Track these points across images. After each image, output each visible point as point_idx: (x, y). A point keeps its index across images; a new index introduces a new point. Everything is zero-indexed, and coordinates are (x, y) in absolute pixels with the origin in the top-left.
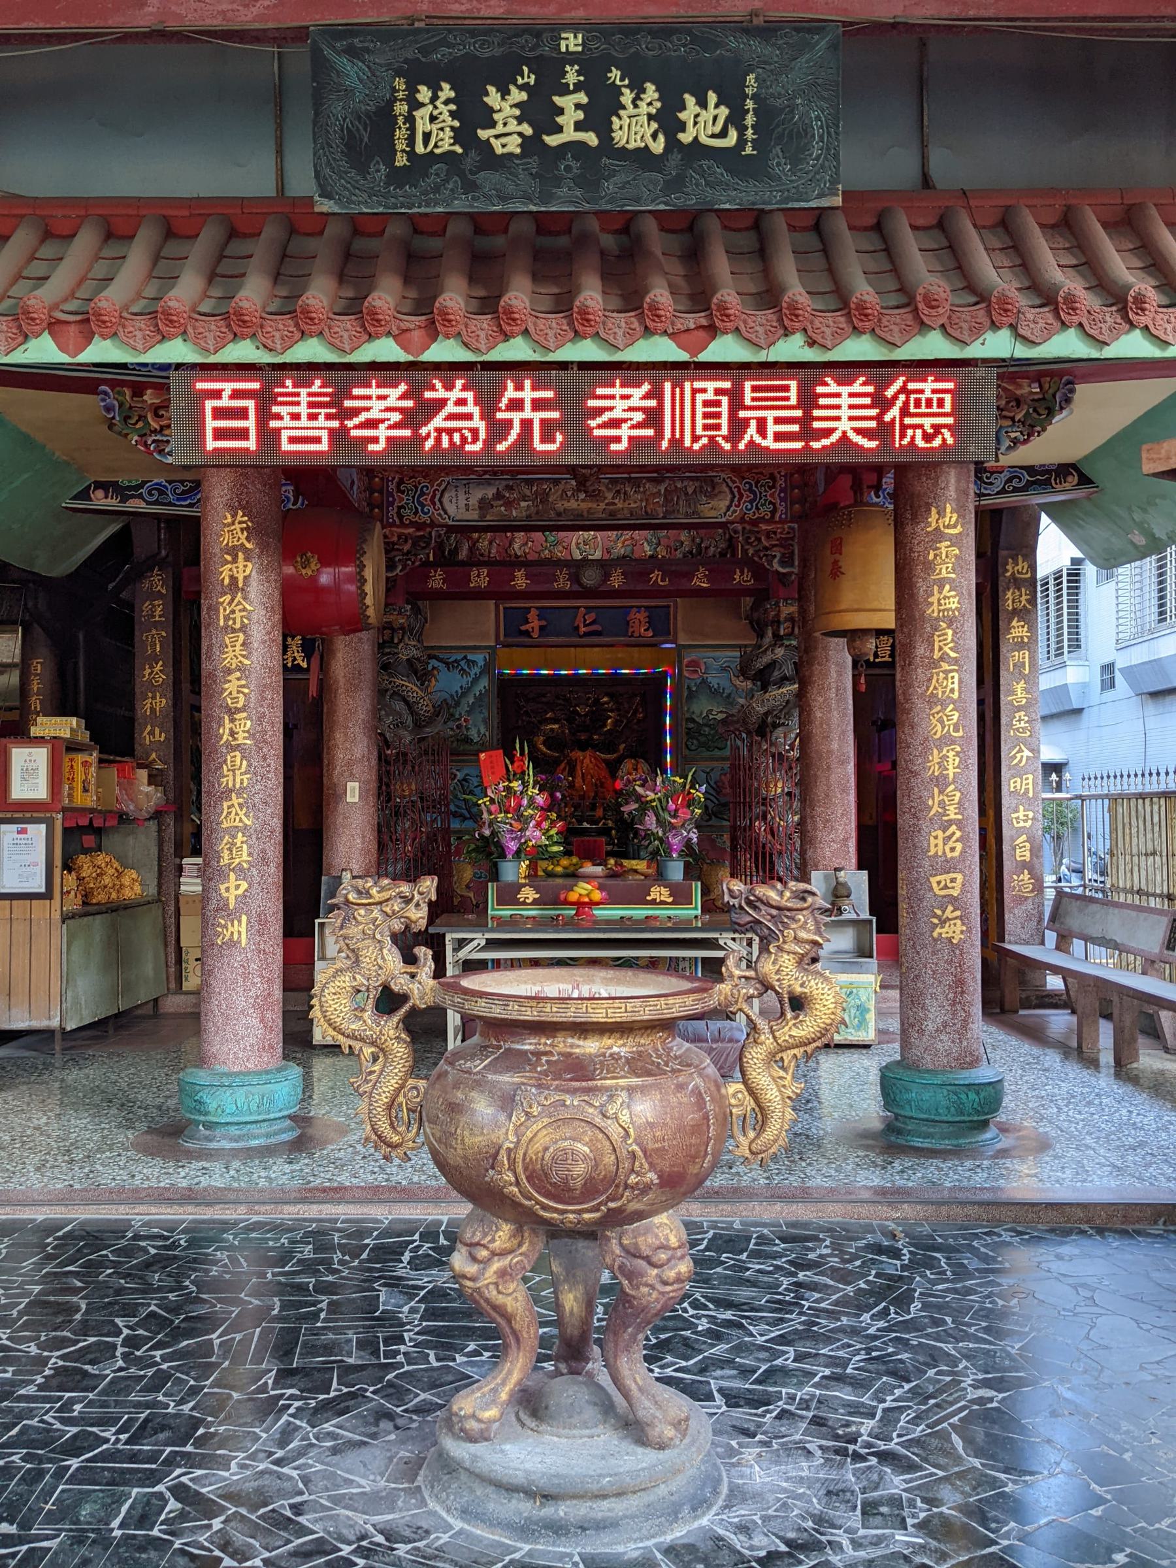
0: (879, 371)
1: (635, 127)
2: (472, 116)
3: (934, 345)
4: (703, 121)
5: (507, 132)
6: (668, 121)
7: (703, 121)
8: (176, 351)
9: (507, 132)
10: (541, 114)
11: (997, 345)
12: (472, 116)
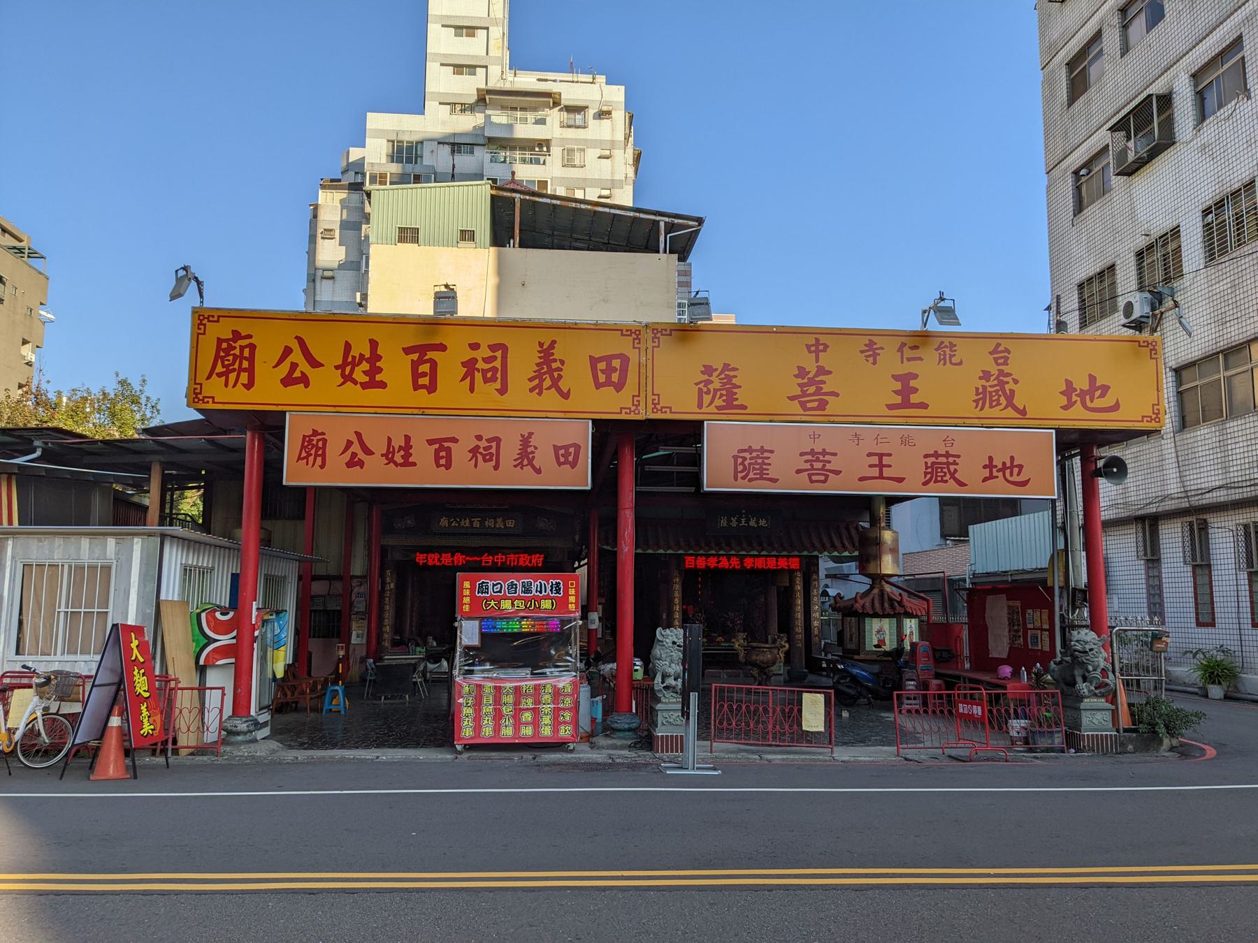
0: (788, 557)
1: (752, 523)
2: (729, 521)
3: (796, 553)
4: (763, 523)
5: (734, 524)
6: (757, 523)
7: (763, 523)
8: (681, 552)
9: (734, 524)
10: (739, 521)
11: (805, 553)
12: (729, 521)
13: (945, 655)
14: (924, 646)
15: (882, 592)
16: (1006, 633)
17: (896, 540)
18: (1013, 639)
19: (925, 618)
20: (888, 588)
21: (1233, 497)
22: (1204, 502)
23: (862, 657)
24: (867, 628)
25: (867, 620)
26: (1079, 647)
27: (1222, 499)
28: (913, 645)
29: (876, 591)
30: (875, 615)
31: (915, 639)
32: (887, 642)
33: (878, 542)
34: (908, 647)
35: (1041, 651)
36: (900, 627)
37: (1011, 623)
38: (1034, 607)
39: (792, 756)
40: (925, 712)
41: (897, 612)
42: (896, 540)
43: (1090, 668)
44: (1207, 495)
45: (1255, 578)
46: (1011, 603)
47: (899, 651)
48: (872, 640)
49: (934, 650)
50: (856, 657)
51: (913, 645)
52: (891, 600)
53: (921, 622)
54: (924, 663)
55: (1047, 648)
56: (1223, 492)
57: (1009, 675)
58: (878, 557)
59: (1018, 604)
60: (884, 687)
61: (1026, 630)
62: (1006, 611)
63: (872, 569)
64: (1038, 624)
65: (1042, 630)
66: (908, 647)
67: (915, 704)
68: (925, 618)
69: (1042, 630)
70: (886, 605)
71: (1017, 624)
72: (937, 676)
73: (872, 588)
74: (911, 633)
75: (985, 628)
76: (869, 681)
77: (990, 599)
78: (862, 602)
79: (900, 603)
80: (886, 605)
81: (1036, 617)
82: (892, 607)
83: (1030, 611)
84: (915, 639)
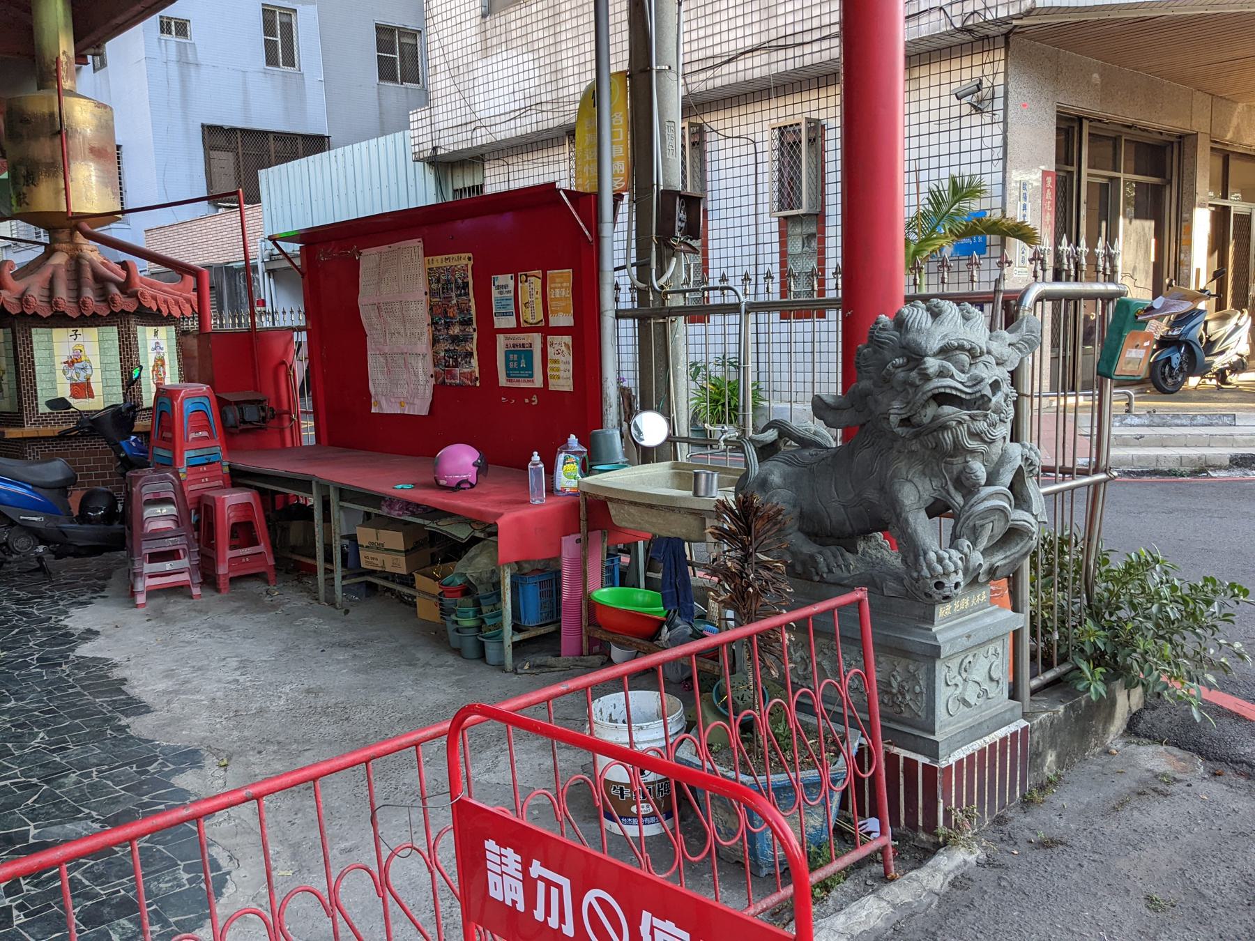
13: (251, 414)
14: (195, 397)
15: (77, 262)
16: (424, 345)
17: (106, 127)
18: (445, 364)
19: (192, 325)
20: (92, 252)
21: (781, 67)
22: (718, 83)
23: (29, 430)
24: (39, 354)
25: (38, 335)
26: (957, 382)
27: (757, 74)
28: (163, 394)
29: (60, 259)
30: (59, 320)
31: (171, 378)
32: (97, 387)
33: (57, 129)
34: (148, 399)
35: (544, 392)
36: (128, 350)
37: (440, 317)
38: (516, 267)
39: (244, 293)
40: (209, 580)
41: (114, 305)
42: (106, 127)
43: (979, 469)
44: (725, 69)
45: (4, 405)
46: (438, 261)
47: (123, 417)
48: (54, 382)
49: (222, 403)
50: (12, 433)
51: (163, 394)
52: (101, 281)
53: (182, 334)
54: (196, 447)
55: (563, 381)
56: (759, 59)
57: (471, 475)
58: (59, 167)
59: (463, 261)
60: (83, 518)
61: (488, 335)
62: (421, 286)
63: (45, 198)
64: (533, 315)
65: (547, 330)
66: (148, 399)
67: (180, 570)
68: (192, 325)
69: (547, 330)
70: (89, 293)
71: (461, 320)
72: (238, 478)
73: (50, 251)
74: (160, 362)
75: (359, 336)
76: (35, 507)
77: (369, 259)
78: (18, 286)
79: (126, 287)
80: (89, 293)
81: (530, 296)
82: (104, 296)
83: (505, 280)
84: (171, 378)
